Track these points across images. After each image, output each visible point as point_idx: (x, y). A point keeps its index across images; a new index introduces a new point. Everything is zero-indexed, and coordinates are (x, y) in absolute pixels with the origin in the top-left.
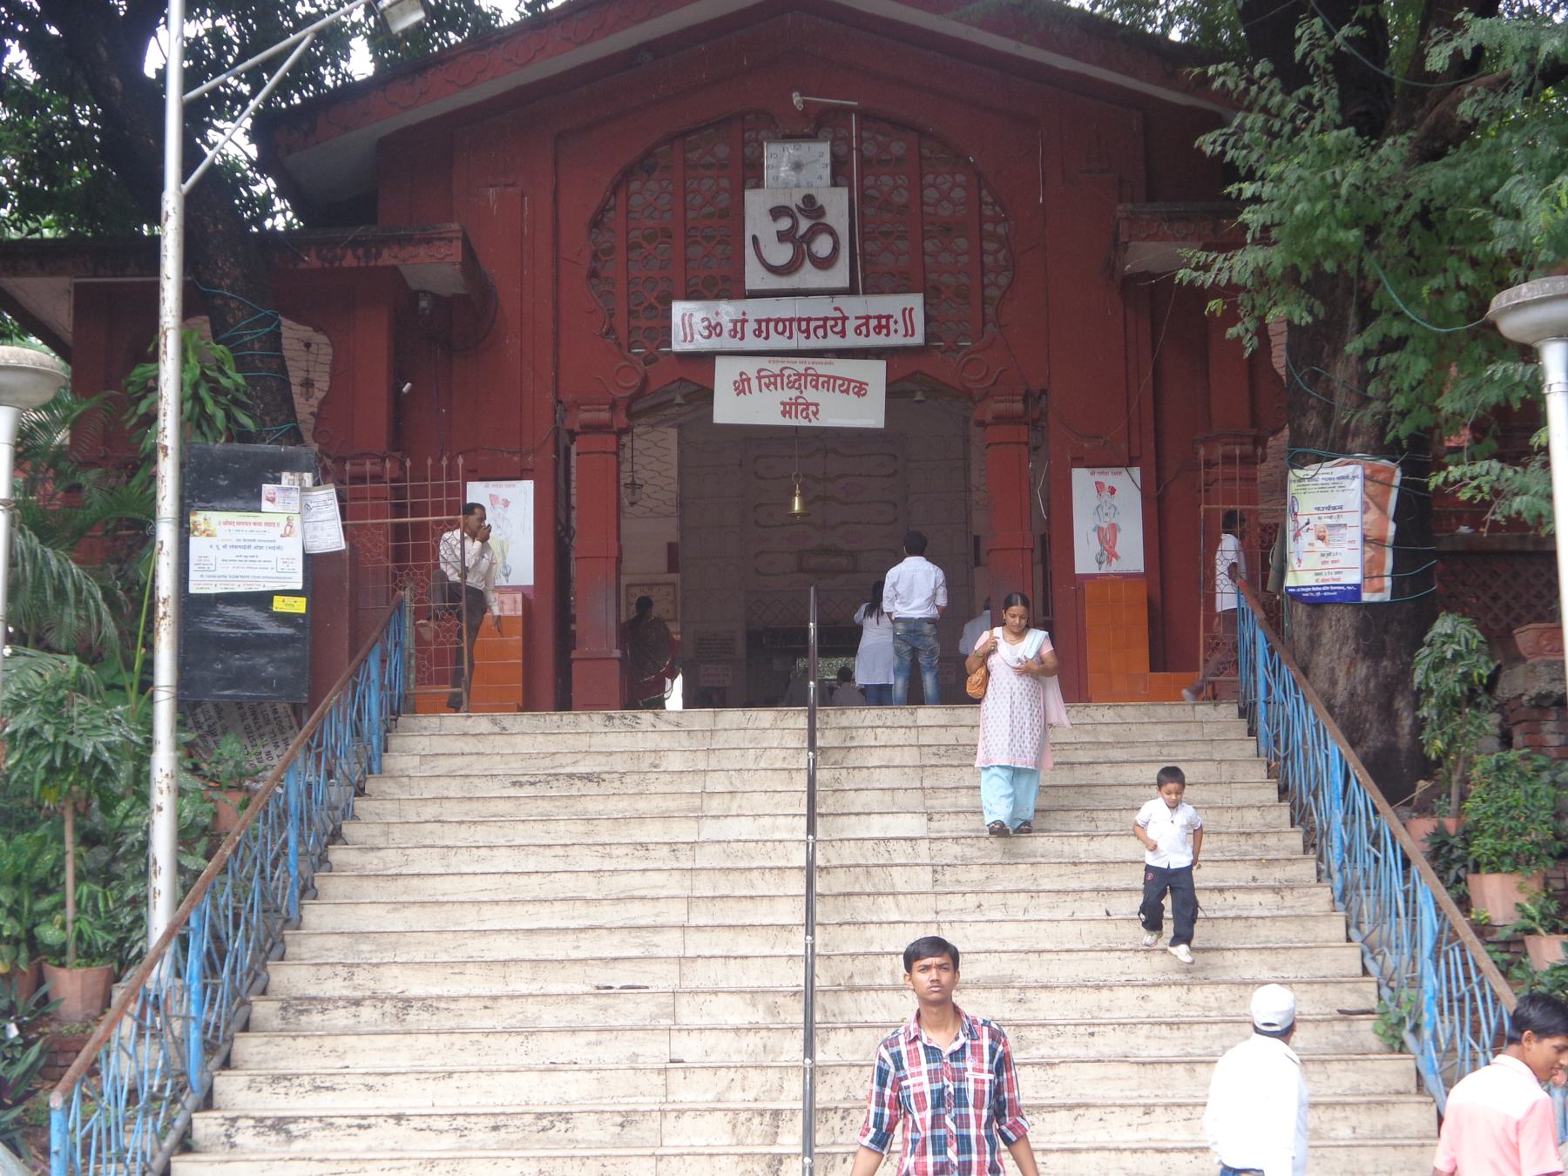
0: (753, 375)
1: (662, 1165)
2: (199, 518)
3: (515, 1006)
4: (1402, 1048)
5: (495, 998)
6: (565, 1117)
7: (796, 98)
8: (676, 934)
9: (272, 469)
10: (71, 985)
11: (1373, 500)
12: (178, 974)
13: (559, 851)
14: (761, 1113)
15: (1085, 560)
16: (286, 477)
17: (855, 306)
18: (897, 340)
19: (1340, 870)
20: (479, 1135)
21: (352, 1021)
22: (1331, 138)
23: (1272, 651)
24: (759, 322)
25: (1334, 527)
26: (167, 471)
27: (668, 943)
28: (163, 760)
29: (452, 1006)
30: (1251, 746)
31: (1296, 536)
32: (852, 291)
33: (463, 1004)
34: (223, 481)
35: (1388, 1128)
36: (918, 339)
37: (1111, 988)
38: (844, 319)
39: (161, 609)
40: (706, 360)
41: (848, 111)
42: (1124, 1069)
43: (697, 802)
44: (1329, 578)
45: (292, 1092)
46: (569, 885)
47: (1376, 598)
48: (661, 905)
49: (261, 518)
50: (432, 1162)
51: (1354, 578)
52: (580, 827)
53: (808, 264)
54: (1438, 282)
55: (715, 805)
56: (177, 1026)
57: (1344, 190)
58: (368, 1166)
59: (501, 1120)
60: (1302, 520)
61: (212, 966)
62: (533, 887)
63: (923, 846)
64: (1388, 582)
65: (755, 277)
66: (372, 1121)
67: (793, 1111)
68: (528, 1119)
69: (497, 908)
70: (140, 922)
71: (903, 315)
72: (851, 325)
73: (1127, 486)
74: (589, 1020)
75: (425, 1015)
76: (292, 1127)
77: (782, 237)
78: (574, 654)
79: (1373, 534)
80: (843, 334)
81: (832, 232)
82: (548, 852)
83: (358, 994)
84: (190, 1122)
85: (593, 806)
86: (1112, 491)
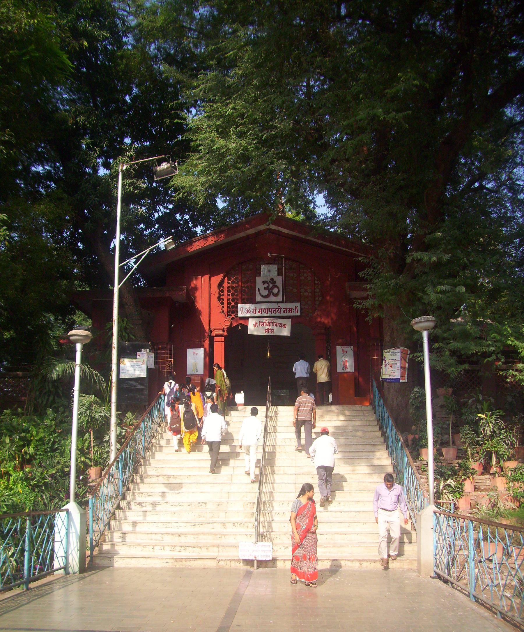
0: (258, 322)
2: (122, 360)
6: (205, 503)
9: (139, 348)
11: (403, 358)
12: (117, 469)
16: (143, 350)
17: (283, 306)
18: (293, 314)
22: (388, 275)
26: (115, 352)
31: (385, 366)
32: (282, 302)
34: (128, 351)
36: (299, 314)
40: (247, 318)
41: (282, 257)
44: (392, 376)
47: (403, 381)
50: (174, 513)
51: (398, 376)
54: (414, 308)
56: (117, 480)
59: (190, 504)
60: (387, 362)
61: (125, 467)
64: (406, 378)
65: (259, 298)
68: (197, 503)
70: (108, 456)
72: (282, 310)
73: (350, 350)
77: (265, 288)
79: (403, 366)
80: (280, 312)
83: (158, 474)
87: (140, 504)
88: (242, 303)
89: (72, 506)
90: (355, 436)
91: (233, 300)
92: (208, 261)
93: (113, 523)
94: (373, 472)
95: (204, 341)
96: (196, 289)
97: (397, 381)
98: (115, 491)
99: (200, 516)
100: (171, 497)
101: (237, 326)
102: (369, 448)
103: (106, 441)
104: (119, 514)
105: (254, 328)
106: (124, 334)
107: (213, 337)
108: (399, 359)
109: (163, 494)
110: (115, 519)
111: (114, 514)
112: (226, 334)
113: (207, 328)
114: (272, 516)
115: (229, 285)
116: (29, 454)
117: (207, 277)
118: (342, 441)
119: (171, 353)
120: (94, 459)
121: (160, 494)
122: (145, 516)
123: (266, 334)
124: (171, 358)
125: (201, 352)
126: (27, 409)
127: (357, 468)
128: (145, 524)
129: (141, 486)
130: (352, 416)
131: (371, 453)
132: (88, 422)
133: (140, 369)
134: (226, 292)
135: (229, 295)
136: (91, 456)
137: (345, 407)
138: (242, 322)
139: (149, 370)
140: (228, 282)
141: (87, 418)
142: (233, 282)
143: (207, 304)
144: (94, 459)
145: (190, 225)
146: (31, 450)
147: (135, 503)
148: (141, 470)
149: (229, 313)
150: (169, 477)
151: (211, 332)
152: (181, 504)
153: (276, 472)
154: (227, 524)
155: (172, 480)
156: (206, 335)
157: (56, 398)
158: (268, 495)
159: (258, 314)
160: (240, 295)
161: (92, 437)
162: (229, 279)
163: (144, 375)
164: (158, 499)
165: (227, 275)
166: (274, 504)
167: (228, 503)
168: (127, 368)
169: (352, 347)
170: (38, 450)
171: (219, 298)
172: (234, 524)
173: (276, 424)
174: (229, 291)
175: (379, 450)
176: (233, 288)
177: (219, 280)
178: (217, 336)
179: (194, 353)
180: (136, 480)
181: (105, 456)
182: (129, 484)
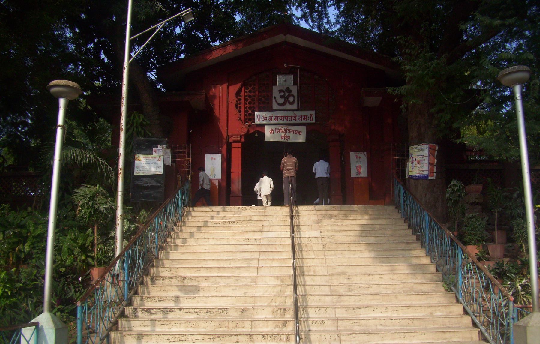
0: (274, 129)
1: (253, 323)
3: (213, 279)
4: (451, 290)
5: (208, 277)
6: (227, 310)
7: (285, 65)
8: (256, 261)
9: (155, 144)
10: (95, 273)
11: (431, 154)
13: (226, 240)
14: (281, 309)
15: (353, 174)
16: (159, 146)
17: (299, 113)
18: (308, 121)
19: (428, 245)
20: (203, 315)
21: (170, 283)
23: (405, 192)
24: (276, 117)
25: (421, 162)
27: (254, 263)
28: (119, 212)
29: (197, 279)
30: (399, 216)
31: (412, 163)
32: (298, 110)
33: (199, 278)
35: (451, 312)
36: (314, 121)
37: (373, 275)
38: (296, 116)
39: (120, 171)
40: (263, 126)
42: (378, 297)
43: (261, 228)
44: (420, 173)
45: (153, 301)
46: (229, 248)
47: (432, 178)
48: (252, 253)
49: (153, 156)
50: (189, 322)
51: (426, 173)
52: (232, 234)
53: (288, 104)
55: (266, 229)
57: (431, 69)
58: (172, 323)
59: (208, 310)
60: (414, 159)
62: (219, 249)
63: (320, 239)
64: (435, 174)
65: (275, 106)
66: (173, 310)
67: (289, 308)
68: (216, 310)
69: (210, 254)
71: (310, 115)
72: (298, 118)
73: (363, 156)
74: (233, 283)
75: (189, 281)
76: (152, 311)
77: (281, 97)
78: (231, 195)
79: (431, 162)
80: (296, 120)
81: (293, 96)
82: (223, 240)
83: (172, 275)
84: (124, 309)
85: (235, 229)
86: (360, 157)
87: (148, 310)
88: (259, 111)
89: (45, 319)
90: (384, 234)
91: (250, 108)
92: (226, 71)
93: (113, 335)
94: (414, 272)
95: (222, 147)
96: (214, 97)
97: (426, 177)
98: (118, 295)
99: (221, 326)
100: (185, 303)
101: (254, 133)
102: (403, 246)
103: (112, 237)
104: (122, 322)
105: (269, 135)
106: (140, 130)
107: (231, 143)
108: (427, 155)
109: (177, 299)
110: (117, 329)
111: (116, 323)
112: (243, 140)
113: (224, 134)
114: (308, 326)
115: (246, 94)
116: (24, 252)
117: (225, 86)
118: (372, 239)
119: (189, 152)
120: (98, 258)
121: (174, 299)
122: (154, 325)
123: (282, 140)
124: (189, 157)
125: (218, 158)
126: (35, 207)
127: (396, 267)
128: (153, 336)
129: (151, 289)
130: (377, 215)
131: (407, 252)
132: (91, 215)
133: (156, 165)
134: (243, 101)
135: (246, 104)
136: (95, 254)
137: (368, 207)
138: (259, 129)
139: (165, 167)
140: (245, 92)
141: (89, 210)
142: (250, 92)
143: (225, 111)
144: (98, 258)
145: (209, 40)
146: (27, 248)
147: (143, 309)
148: (153, 271)
149: (246, 120)
150: (185, 278)
151: (229, 138)
152: (198, 310)
153: (306, 273)
154: (254, 337)
155: (188, 283)
156: (224, 141)
157: (66, 195)
158: (301, 300)
159: (274, 122)
160: (257, 104)
161: (96, 232)
162: (246, 89)
163: (160, 172)
164: (171, 304)
165: (245, 84)
166: (310, 310)
167: (254, 309)
168: (143, 165)
169: (366, 153)
170: (34, 248)
171: (237, 106)
172: (263, 336)
173: (299, 222)
174: (246, 100)
175: (415, 249)
176: (250, 97)
177: (237, 89)
178: (235, 142)
179: (212, 158)
180: (147, 282)
181: (110, 254)
182: (138, 287)
